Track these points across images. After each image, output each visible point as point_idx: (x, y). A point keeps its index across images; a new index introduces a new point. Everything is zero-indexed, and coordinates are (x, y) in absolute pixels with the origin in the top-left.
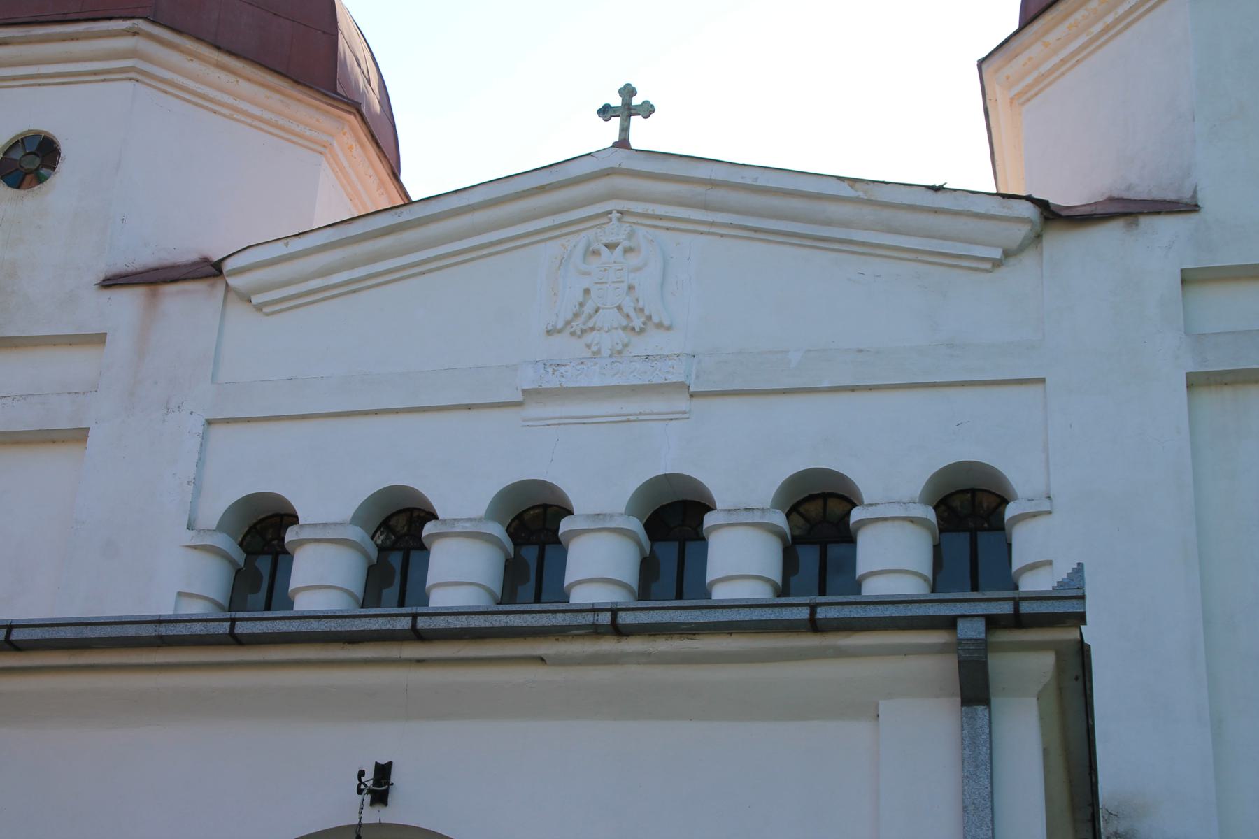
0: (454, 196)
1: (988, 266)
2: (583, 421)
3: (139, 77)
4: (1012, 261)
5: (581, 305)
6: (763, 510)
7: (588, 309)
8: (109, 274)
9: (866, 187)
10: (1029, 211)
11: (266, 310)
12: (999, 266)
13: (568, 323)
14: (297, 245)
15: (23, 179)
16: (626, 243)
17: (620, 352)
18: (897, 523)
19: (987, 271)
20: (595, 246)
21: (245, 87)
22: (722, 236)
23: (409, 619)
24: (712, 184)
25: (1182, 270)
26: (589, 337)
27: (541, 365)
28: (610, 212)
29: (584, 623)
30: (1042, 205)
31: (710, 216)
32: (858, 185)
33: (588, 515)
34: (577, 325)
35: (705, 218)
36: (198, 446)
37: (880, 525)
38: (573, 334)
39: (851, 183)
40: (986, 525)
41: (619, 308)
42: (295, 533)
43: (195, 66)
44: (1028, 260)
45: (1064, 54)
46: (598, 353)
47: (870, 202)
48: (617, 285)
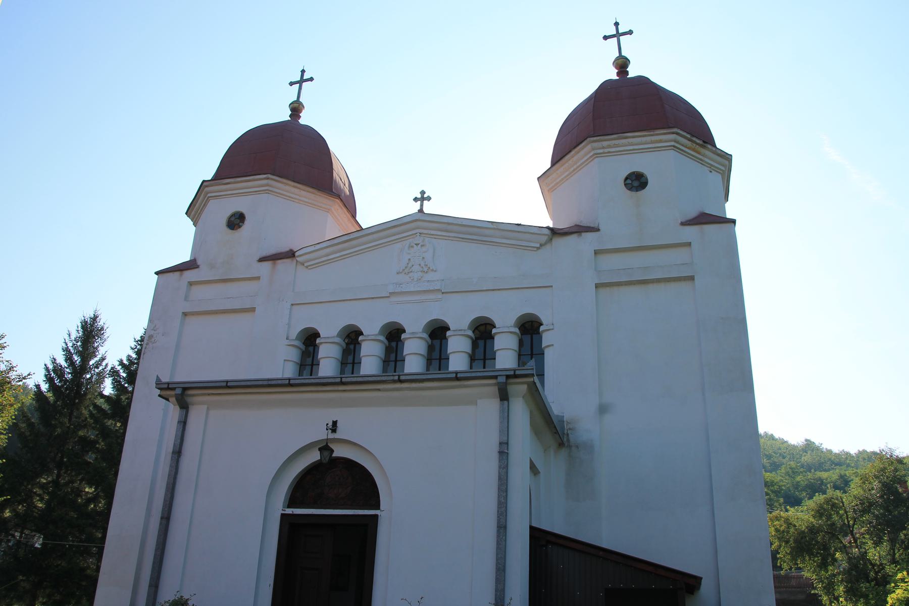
1: (535, 249)
4: (543, 247)
5: (408, 264)
7: (410, 265)
8: (261, 257)
10: (548, 232)
11: (309, 268)
13: (404, 270)
14: (318, 247)
16: (422, 244)
17: (420, 279)
19: (535, 251)
21: (303, 193)
24: (449, 224)
26: (411, 274)
34: (406, 271)
37: (501, 334)
38: (405, 273)
43: (287, 188)
44: (548, 247)
46: (413, 279)
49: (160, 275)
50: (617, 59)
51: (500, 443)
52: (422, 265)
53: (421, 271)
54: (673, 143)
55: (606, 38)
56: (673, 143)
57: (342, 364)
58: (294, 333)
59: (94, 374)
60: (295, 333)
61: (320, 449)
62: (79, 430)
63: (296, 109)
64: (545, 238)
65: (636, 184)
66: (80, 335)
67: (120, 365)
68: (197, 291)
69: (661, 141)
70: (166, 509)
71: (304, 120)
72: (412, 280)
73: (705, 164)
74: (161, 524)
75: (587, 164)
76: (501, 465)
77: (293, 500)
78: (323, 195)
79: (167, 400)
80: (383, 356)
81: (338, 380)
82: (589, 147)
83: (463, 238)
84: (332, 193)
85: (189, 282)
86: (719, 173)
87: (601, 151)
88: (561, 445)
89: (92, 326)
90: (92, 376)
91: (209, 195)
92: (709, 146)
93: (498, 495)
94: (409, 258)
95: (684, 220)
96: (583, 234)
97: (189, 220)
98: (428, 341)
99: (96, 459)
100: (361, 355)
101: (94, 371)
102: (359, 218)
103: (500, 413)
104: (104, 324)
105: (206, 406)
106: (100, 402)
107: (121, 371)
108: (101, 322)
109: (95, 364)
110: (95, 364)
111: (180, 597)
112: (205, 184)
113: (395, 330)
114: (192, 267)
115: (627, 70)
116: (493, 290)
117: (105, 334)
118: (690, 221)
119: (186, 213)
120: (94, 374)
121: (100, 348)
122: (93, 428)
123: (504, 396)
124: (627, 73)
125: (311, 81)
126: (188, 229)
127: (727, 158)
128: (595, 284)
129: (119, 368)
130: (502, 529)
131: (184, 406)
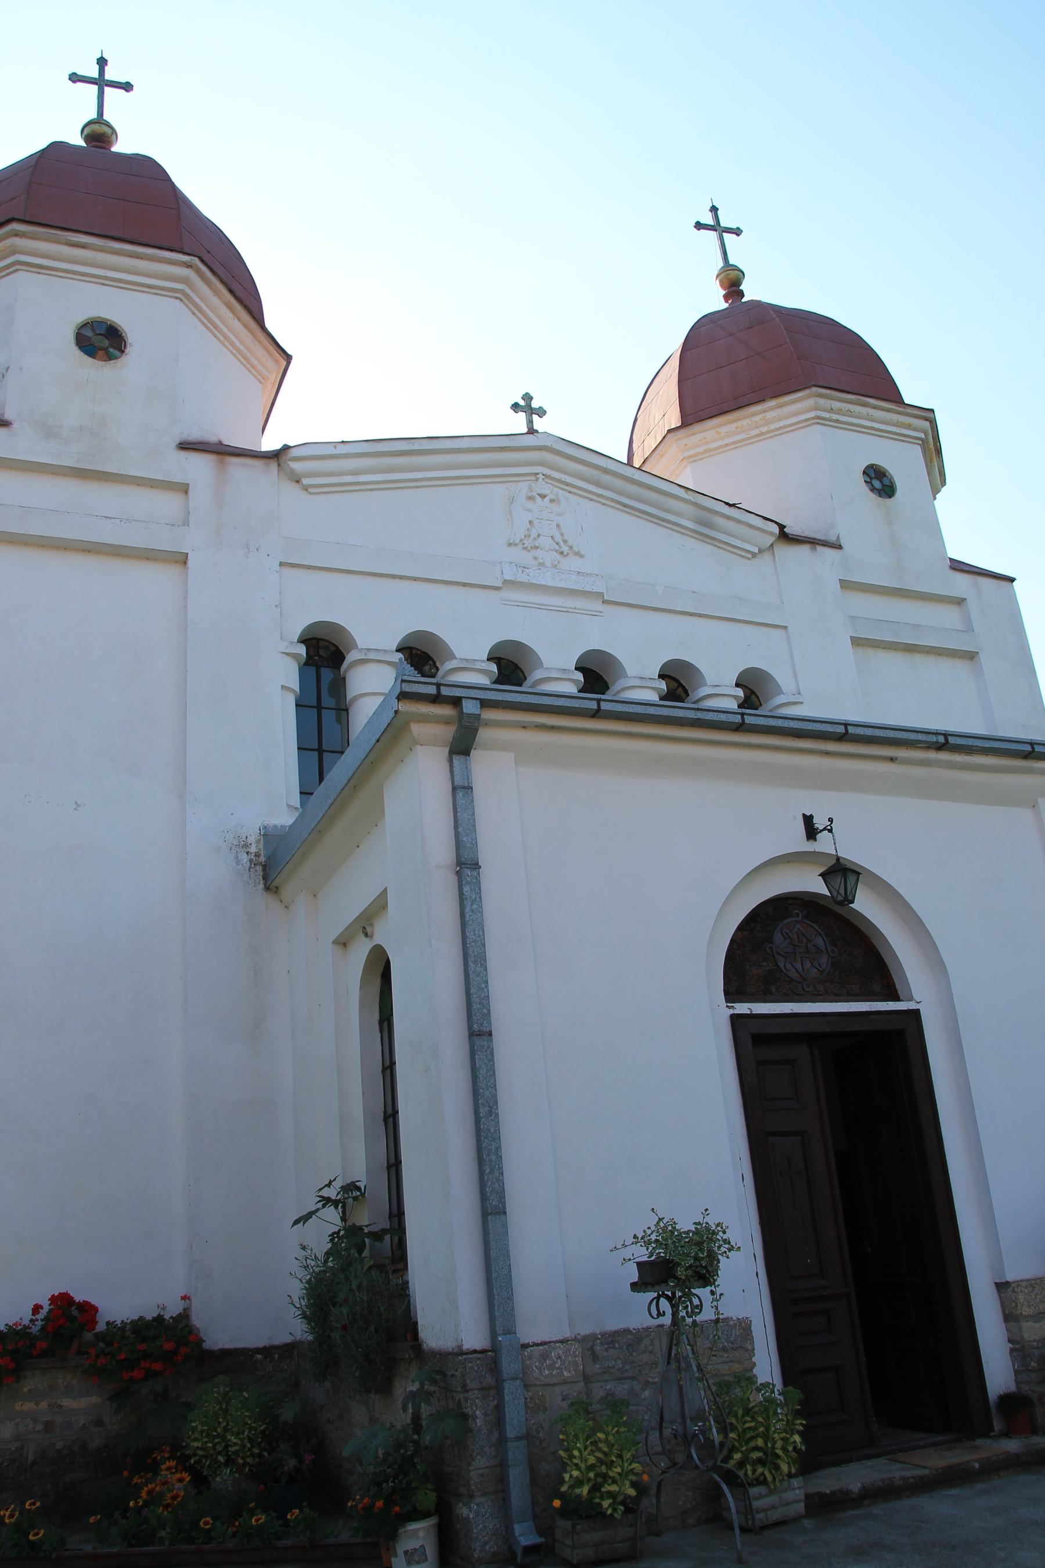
0: (404, 442)
2: (540, 607)
7: (534, 533)
10: (776, 529)
11: (310, 490)
16: (552, 496)
19: (749, 559)
21: (237, 325)
24: (605, 471)
26: (538, 553)
28: (538, 474)
30: (782, 527)
31: (600, 491)
33: (558, 669)
34: (528, 543)
35: (596, 491)
40: (746, 706)
42: (364, 654)
43: (215, 301)
44: (767, 557)
45: (726, 441)
69: (909, 427)
81: (738, 719)
82: (810, 402)
87: (827, 415)
124: (741, 294)
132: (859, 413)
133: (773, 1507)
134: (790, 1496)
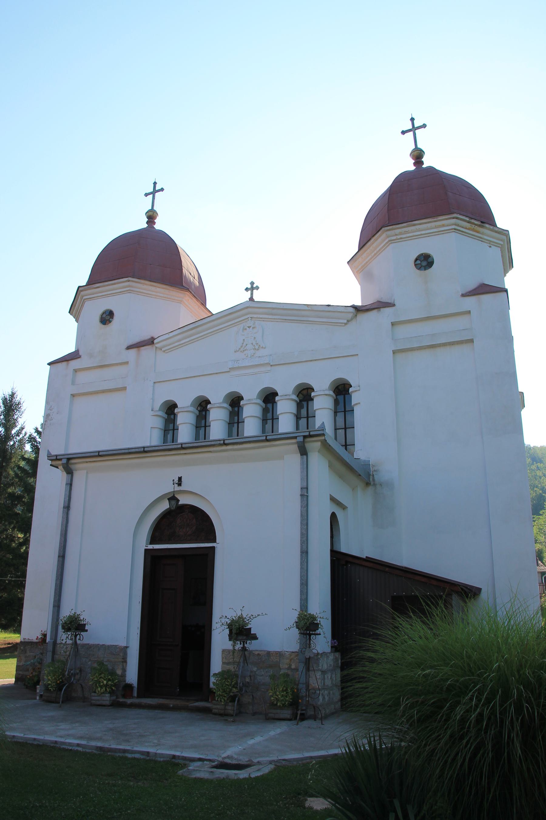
1: (344, 325)
3: (131, 292)
4: (350, 323)
5: (243, 344)
6: (289, 395)
7: (244, 345)
8: (128, 346)
9: (311, 306)
10: (352, 310)
12: (346, 324)
13: (240, 349)
14: (171, 335)
15: (106, 322)
16: (253, 326)
17: (253, 356)
18: (323, 396)
20: (245, 327)
21: (158, 289)
22: (277, 322)
23: (181, 445)
25: (391, 322)
26: (245, 352)
27: (233, 361)
28: (249, 318)
29: (218, 443)
32: (309, 306)
33: (247, 400)
34: (242, 349)
36: (152, 389)
37: (318, 396)
38: (241, 351)
39: (307, 305)
41: (252, 344)
43: (145, 286)
46: (247, 356)
47: (312, 310)
48: (251, 338)
49: (52, 365)
50: (413, 151)
51: (301, 488)
52: (253, 344)
53: (254, 349)
54: (453, 227)
55: (403, 133)
56: (453, 227)
57: (196, 427)
58: (157, 406)
59: (17, 441)
60: (158, 404)
61: (169, 499)
62: (8, 488)
63: (151, 217)
64: (350, 316)
65: (424, 263)
66: (2, 409)
67: (36, 432)
68: (82, 377)
69: (443, 226)
70: (62, 550)
71: (159, 226)
72: (247, 356)
73: (485, 241)
74: (58, 561)
75: (385, 249)
76: (302, 506)
77: (153, 540)
78: (174, 290)
79: (57, 467)
80: (228, 420)
82: (384, 235)
83: (285, 320)
84: (183, 287)
85: (74, 369)
86: (499, 247)
87: (394, 238)
88: (368, 484)
89: (11, 401)
90: (15, 443)
91: (85, 298)
92: (487, 226)
93: (301, 528)
94: (243, 339)
95: (464, 293)
96: (382, 309)
97: (72, 317)
98: (262, 405)
99: (23, 510)
100: (210, 420)
101: (16, 438)
102: (208, 306)
103: (301, 465)
104: (20, 399)
105: (86, 471)
106: (22, 464)
107: (37, 437)
108: (17, 397)
109: (16, 433)
110: (16, 433)
111: (73, 613)
112: (80, 289)
113: (236, 397)
114: (75, 358)
115: (422, 160)
116: (311, 361)
117: (22, 407)
118: (470, 292)
119: (69, 312)
120: (17, 441)
121: (19, 419)
122: (19, 486)
123: (303, 452)
124: (422, 163)
125: (162, 191)
126: (72, 324)
127: (505, 234)
128: (393, 350)
129: (35, 435)
130: (305, 553)
131: (69, 471)
132: (412, 230)
133: (98, 700)
134: (104, 698)
